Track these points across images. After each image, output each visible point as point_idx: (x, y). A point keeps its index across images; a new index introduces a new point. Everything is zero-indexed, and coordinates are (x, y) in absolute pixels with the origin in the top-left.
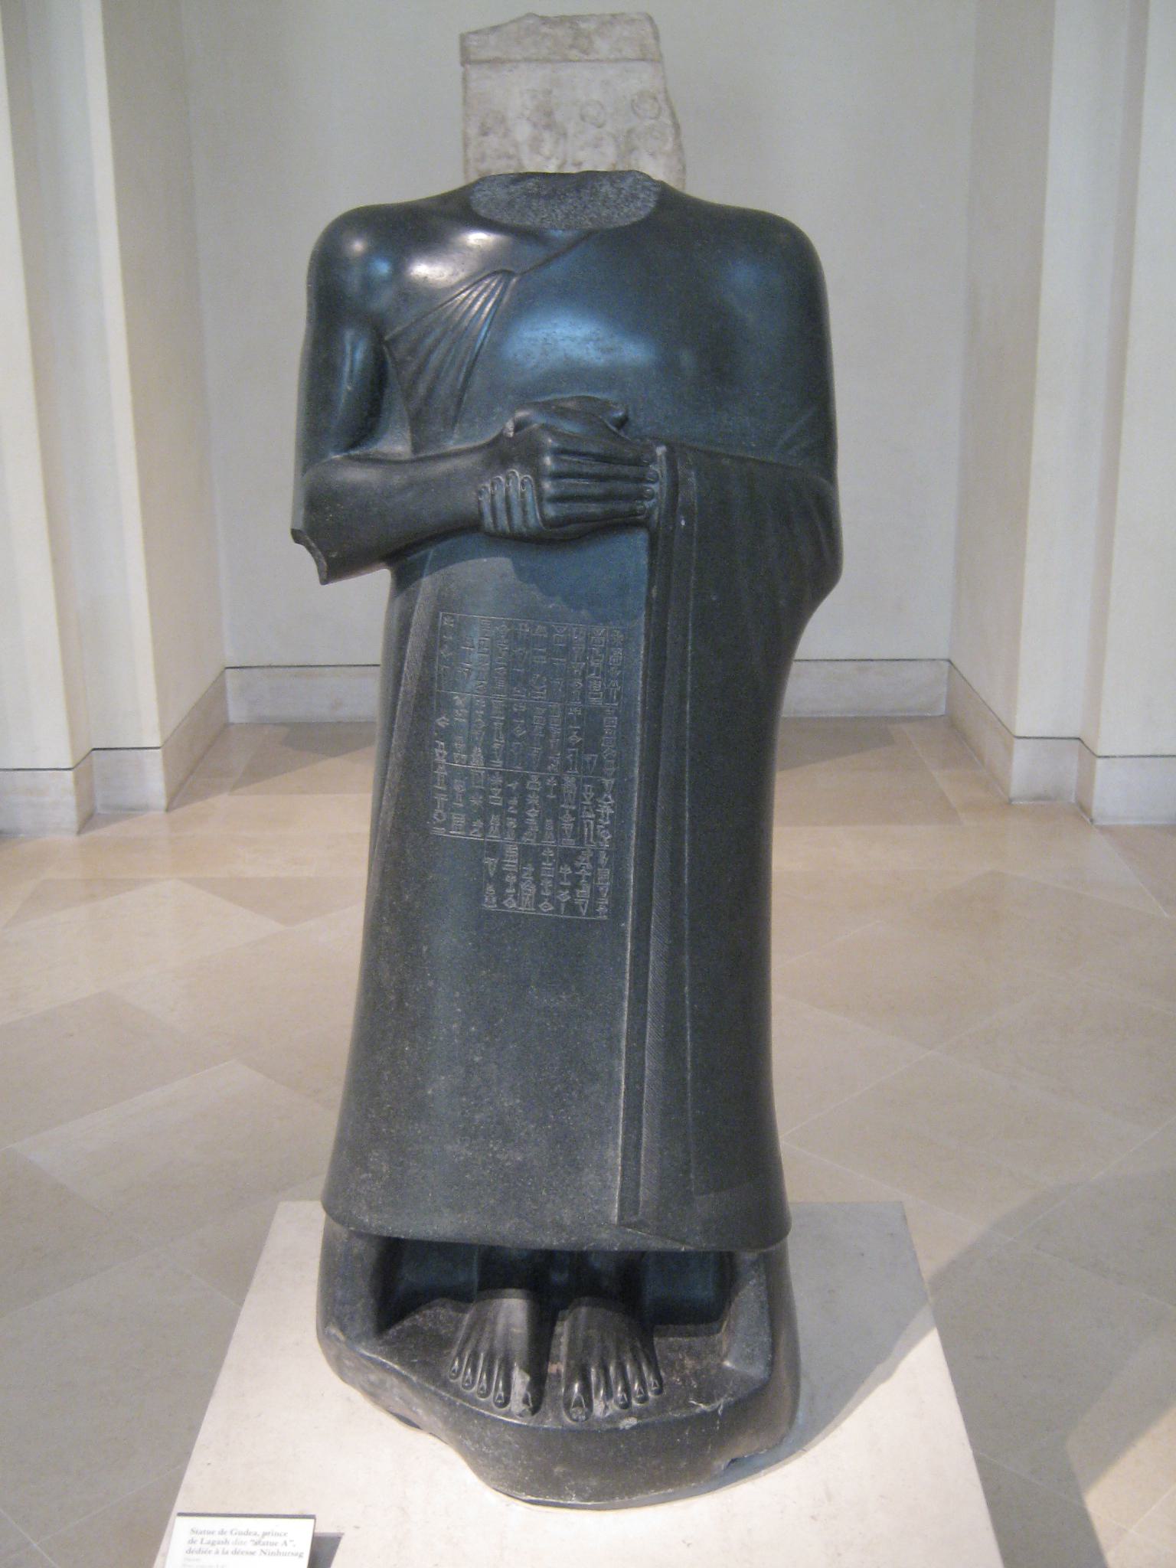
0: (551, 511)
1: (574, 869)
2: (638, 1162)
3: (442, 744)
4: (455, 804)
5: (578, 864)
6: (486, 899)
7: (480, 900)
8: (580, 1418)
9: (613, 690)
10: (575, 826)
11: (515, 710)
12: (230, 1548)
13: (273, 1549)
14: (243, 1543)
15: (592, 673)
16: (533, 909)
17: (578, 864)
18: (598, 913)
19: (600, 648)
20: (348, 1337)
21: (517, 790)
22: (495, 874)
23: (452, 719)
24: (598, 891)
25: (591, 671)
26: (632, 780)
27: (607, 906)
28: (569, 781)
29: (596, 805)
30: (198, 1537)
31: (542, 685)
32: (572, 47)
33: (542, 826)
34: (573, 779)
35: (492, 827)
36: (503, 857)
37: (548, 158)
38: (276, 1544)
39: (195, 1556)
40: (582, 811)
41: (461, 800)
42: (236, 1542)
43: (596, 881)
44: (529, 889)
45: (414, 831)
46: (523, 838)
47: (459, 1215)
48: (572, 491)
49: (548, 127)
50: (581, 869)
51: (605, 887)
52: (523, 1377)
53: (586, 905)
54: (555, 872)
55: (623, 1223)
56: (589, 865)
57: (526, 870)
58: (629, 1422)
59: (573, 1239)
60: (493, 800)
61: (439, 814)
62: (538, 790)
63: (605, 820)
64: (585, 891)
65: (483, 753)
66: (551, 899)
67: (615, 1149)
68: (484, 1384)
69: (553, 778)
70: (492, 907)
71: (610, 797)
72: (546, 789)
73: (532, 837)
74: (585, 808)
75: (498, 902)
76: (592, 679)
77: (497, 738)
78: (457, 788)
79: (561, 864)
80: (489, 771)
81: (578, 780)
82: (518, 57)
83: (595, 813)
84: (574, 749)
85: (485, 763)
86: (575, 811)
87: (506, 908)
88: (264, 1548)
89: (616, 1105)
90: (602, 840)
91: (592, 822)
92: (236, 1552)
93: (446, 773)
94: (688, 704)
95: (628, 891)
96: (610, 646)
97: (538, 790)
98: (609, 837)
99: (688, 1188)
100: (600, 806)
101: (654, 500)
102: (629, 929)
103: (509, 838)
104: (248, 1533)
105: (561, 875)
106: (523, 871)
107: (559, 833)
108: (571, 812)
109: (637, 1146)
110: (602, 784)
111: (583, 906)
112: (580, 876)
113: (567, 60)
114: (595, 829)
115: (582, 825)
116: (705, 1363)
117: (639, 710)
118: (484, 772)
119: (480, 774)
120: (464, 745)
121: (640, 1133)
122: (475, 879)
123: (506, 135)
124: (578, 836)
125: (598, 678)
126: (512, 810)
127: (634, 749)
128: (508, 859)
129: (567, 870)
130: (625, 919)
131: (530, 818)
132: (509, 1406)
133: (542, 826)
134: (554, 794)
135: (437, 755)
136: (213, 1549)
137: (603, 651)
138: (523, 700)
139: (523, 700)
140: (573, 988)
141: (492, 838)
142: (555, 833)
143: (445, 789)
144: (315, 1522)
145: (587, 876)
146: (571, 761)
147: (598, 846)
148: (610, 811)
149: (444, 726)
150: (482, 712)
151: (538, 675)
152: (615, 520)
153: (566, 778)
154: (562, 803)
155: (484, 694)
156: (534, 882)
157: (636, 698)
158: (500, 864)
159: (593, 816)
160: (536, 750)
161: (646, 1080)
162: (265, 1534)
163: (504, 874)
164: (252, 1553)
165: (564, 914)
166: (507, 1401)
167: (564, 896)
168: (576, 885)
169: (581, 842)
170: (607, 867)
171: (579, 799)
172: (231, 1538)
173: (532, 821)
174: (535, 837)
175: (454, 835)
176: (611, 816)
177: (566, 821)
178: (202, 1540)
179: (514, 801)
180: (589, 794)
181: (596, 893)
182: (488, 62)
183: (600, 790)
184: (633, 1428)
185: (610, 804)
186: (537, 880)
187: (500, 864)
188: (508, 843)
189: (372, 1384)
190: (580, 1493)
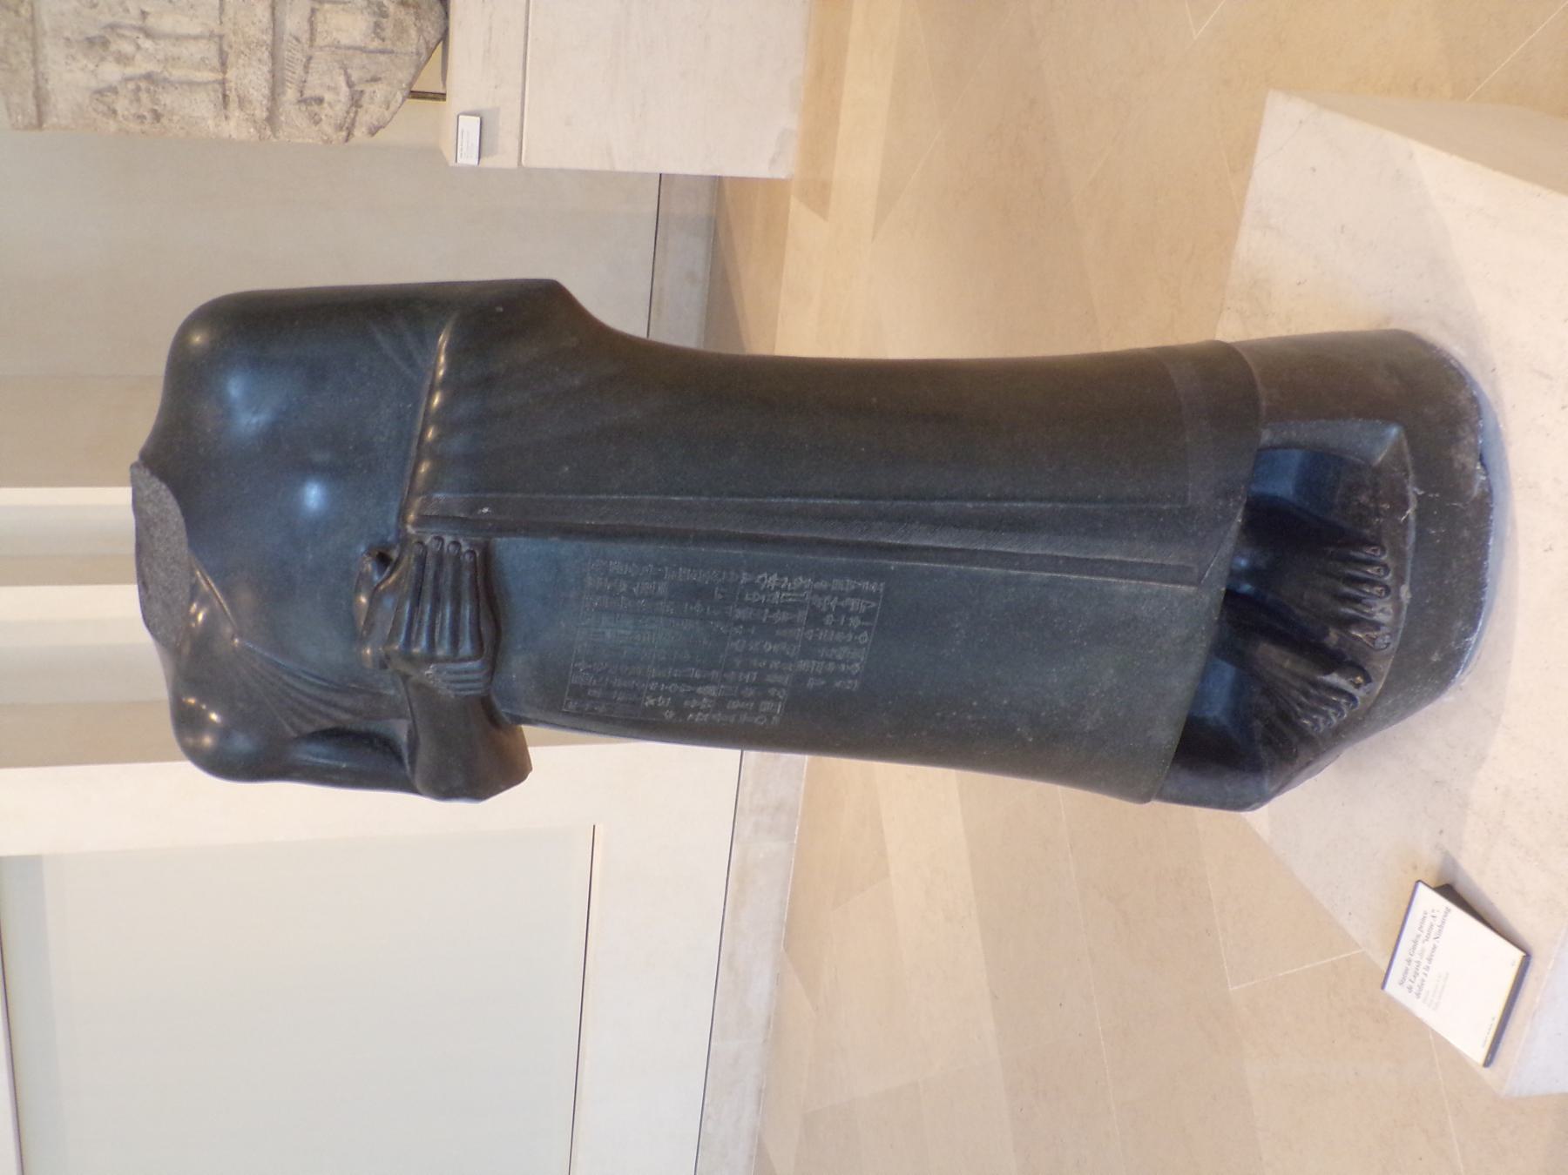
0: (466, 647)
2: (1140, 565)
5: (824, 609)
8: (1386, 641)
12: (1424, 963)
13: (1436, 929)
14: (1423, 950)
25: (631, 591)
27: (871, 582)
28: (740, 614)
29: (767, 590)
30: (1408, 983)
32: (17, 12)
33: (783, 639)
37: (138, 47)
38: (1432, 926)
39: (1423, 993)
42: (1421, 955)
47: (1157, 723)
49: (105, 43)
50: (829, 606)
51: (851, 584)
53: (868, 602)
55: (1198, 582)
56: (827, 598)
58: (1405, 593)
59: (1203, 628)
63: (783, 582)
64: (853, 603)
66: (857, 632)
67: (1121, 584)
69: (735, 629)
75: (853, 678)
79: (822, 625)
82: (32, 71)
83: (774, 591)
86: (770, 610)
88: (1433, 936)
89: (1075, 581)
90: (803, 585)
92: (1430, 960)
94: (673, 498)
99: (1176, 512)
100: (768, 586)
101: (461, 541)
104: (1415, 942)
107: (791, 624)
109: (1122, 564)
110: (747, 584)
111: (868, 605)
113: (33, 20)
114: (792, 591)
115: (787, 604)
116: (1367, 483)
121: (1109, 561)
123: (113, 90)
124: (793, 607)
129: (829, 619)
131: (772, 650)
132: (1358, 698)
133: (783, 639)
136: (1421, 975)
137: (611, 579)
144: (1423, 882)
145: (839, 600)
148: (775, 577)
152: (479, 583)
153: (737, 617)
158: (816, 676)
159: (777, 594)
161: (1056, 553)
162: (1420, 928)
164: (1435, 948)
167: (855, 622)
168: (846, 611)
170: (831, 582)
171: (759, 606)
172: (1416, 958)
173: (776, 648)
176: (780, 576)
178: (1410, 980)
180: (755, 597)
181: (856, 593)
182: (38, 106)
183: (752, 586)
184: (1412, 589)
186: (831, 645)
187: (816, 676)
190: (1466, 635)
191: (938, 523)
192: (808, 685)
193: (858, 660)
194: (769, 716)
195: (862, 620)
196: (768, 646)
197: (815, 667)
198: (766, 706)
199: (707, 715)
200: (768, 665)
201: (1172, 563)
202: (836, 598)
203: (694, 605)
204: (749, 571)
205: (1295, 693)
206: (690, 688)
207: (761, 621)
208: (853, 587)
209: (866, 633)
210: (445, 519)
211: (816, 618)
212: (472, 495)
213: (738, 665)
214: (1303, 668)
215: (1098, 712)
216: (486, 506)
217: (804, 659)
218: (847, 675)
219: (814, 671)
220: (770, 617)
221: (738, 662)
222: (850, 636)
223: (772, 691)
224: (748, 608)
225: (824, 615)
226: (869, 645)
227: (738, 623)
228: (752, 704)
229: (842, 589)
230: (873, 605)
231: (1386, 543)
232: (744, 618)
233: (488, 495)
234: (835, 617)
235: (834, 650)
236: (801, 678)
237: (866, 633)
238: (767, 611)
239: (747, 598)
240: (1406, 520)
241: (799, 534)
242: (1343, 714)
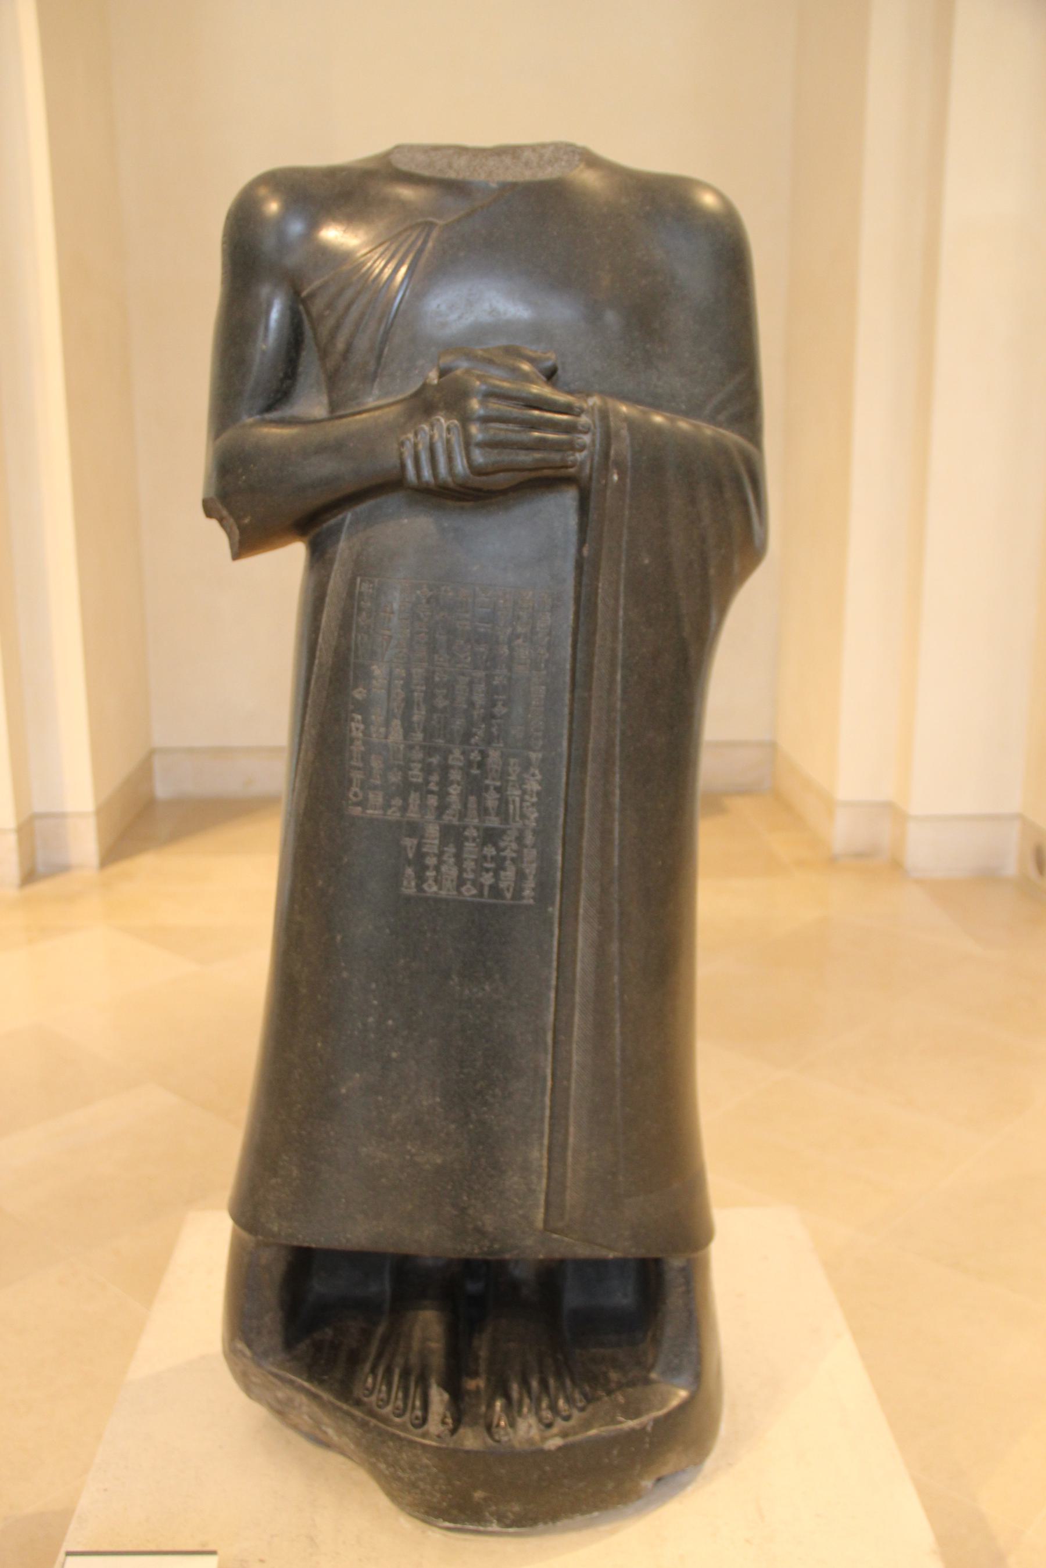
1: (499, 850)
20: (255, 1353)
25: (518, 637)
29: (521, 781)
33: (465, 805)
34: (498, 753)
43: (522, 862)
44: (450, 870)
48: (502, 436)
51: (531, 869)
52: (441, 1395)
56: (514, 846)
58: (554, 1443)
63: (532, 796)
64: (509, 874)
66: (474, 882)
67: (541, 1150)
68: (400, 1403)
69: (476, 752)
72: (470, 764)
73: (454, 816)
79: (484, 844)
83: (521, 788)
89: (542, 1101)
90: (528, 819)
101: (585, 453)
105: (485, 857)
107: (483, 811)
115: (507, 803)
124: (503, 811)
129: (490, 851)
133: (465, 805)
140: (497, 976)
142: (479, 811)
147: (524, 825)
148: (536, 787)
158: (419, 846)
159: (518, 792)
166: (424, 1420)
168: (500, 867)
170: (533, 847)
171: (504, 775)
176: (538, 794)
179: (435, 778)
180: (514, 768)
181: (521, 876)
183: (527, 765)
184: (560, 1449)
186: (459, 858)
187: (419, 846)
189: (279, 1401)
191: (600, 950)
192: (407, 839)
193: (440, 889)
194: (363, 804)
195: (491, 887)
196: (455, 789)
197: (431, 844)
198: (377, 798)
199: (361, 735)
200: (432, 792)
201: (568, 1197)
202: (514, 855)
203: (503, 705)
204: (543, 760)
205: (399, 1360)
207: (487, 778)
208: (527, 871)
209: (474, 892)
210: (608, 437)
211: (490, 836)
212: (629, 464)
213: (431, 760)
214: (437, 1361)
215: (385, 1156)
216: (620, 479)
217: (440, 831)
218: (421, 879)
219: (426, 844)
220: (492, 788)
221: (435, 760)
222: (471, 876)
223: (397, 802)
224: (501, 763)
225: (495, 845)
226: (461, 898)
227: (484, 754)
228: (378, 782)
229: (525, 859)
230: (509, 895)
231: (590, 1409)
232: (490, 760)
233: (628, 481)
234: (492, 858)
235: (452, 860)
236: (415, 829)
237: (474, 892)
238: (498, 784)
239: (512, 761)
240: (620, 1422)
241: (587, 807)
242: (399, 1416)
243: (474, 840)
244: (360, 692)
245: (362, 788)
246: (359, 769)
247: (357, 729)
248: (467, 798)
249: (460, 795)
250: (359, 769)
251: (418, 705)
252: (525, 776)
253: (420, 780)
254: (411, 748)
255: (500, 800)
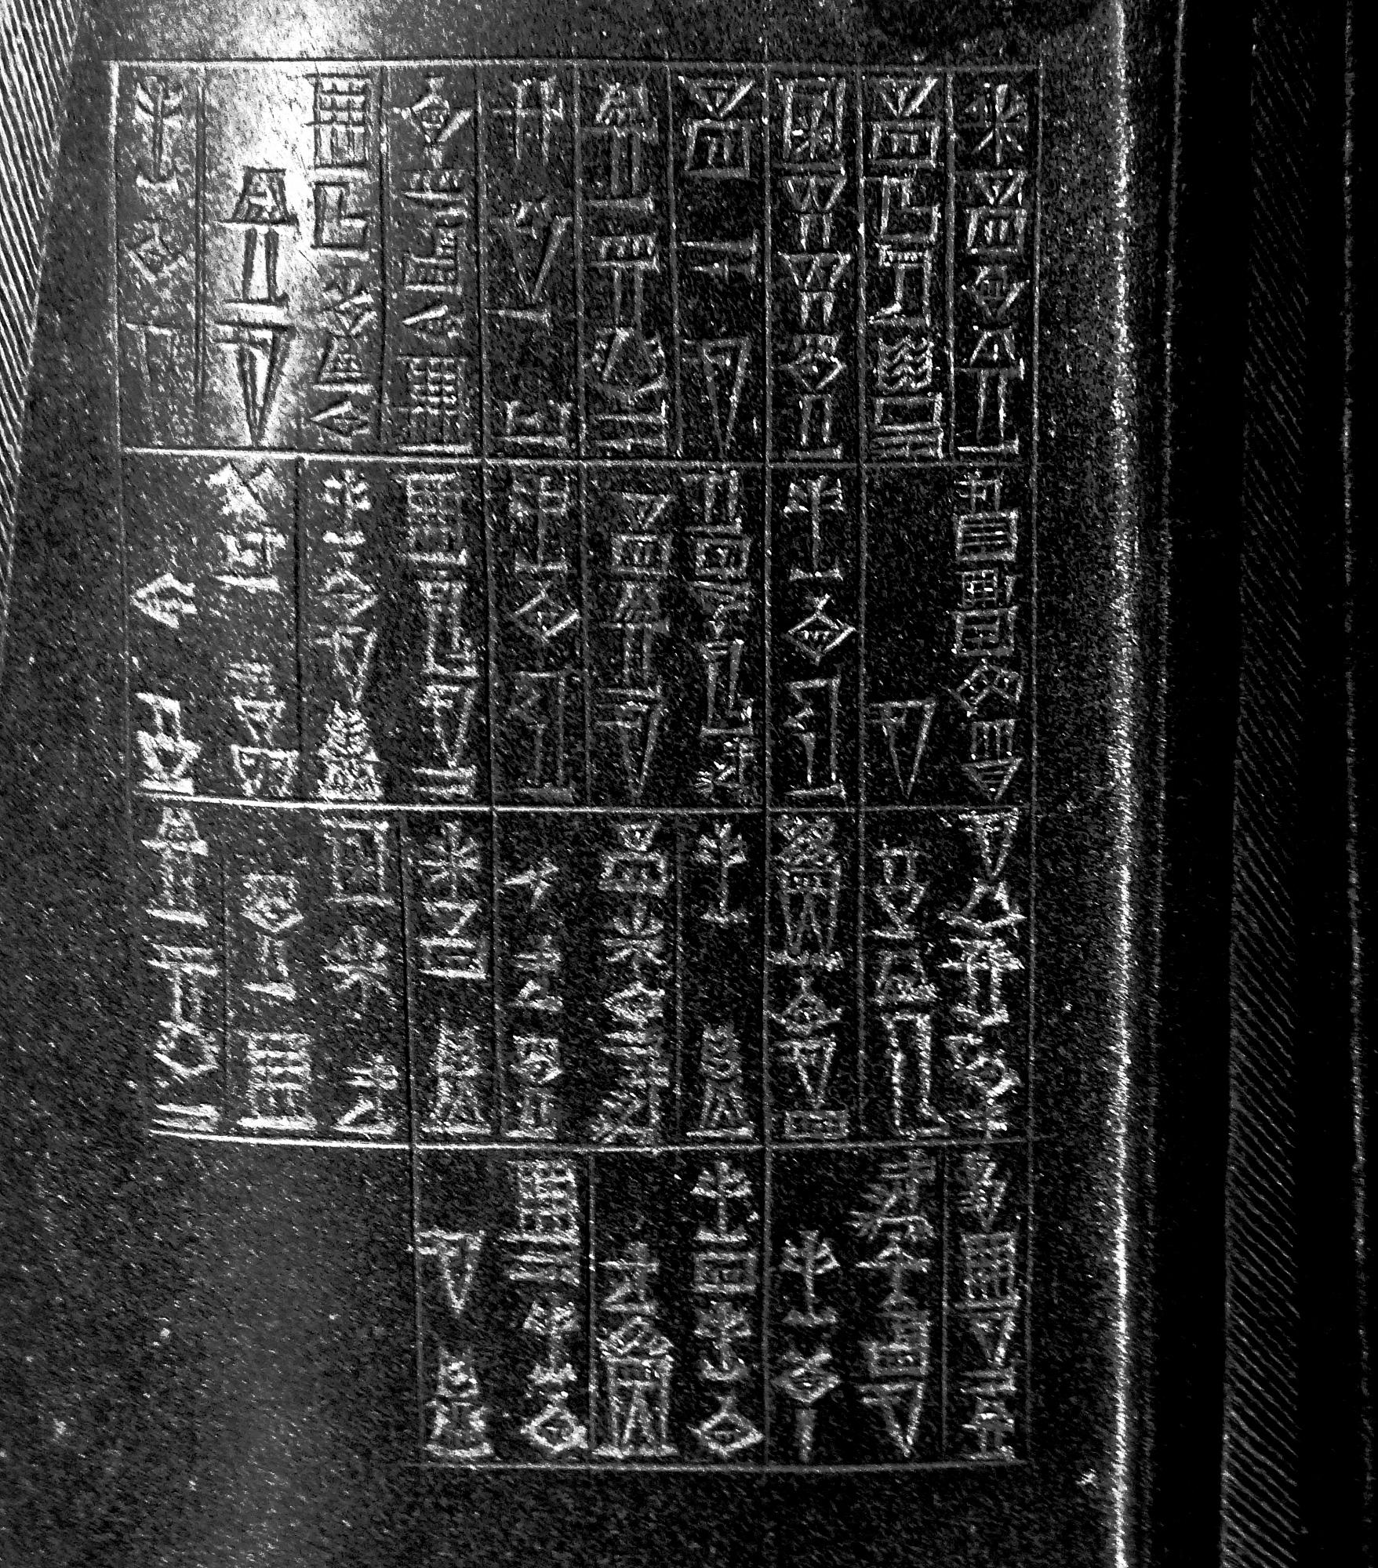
1: (851, 1247)
3: (173, 706)
4: (254, 987)
6: (441, 1421)
7: (416, 1426)
9: (993, 382)
10: (846, 1050)
11: (520, 511)
15: (889, 301)
16: (668, 1450)
17: (861, 1223)
18: (972, 1440)
19: (923, 171)
21: (551, 900)
22: (475, 1301)
23: (208, 586)
24: (970, 1339)
26: (1102, 810)
27: (1012, 1403)
31: (647, 380)
33: (691, 1076)
34: (823, 830)
35: (444, 1087)
36: (509, 1220)
40: (872, 971)
41: (283, 969)
43: (958, 1293)
45: (69, 1126)
46: (602, 1127)
50: (883, 1242)
54: (760, 1270)
56: (918, 1226)
57: (618, 1275)
60: (440, 957)
61: (184, 1038)
62: (658, 890)
65: (377, 739)
66: (750, 1398)
70: (474, 1453)
71: (1001, 896)
73: (641, 1119)
74: (889, 958)
75: (497, 1431)
76: (891, 335)
77: (440, 659)
78: (258, 912)
79: (786, 1229)
80: (414, 820)
81: (845, 826)
83: (934, 975)
84: (818, 683)
85: (388, 784)
86: (843, 976)
87: (539, 1453)
90: (975, 1099)
91: (922, 1022)
93: (200, 847)
95: (1105, 1325)
96: (968, 161)
97: (658, 890)
98: (1005, 1084)
102: (1119, 1492)
103: (525, 1131)
106: (605, 1280)
108: (823, 984)
110: (963, 845)
112: (883, 1276)
115: (878, 1035)
117: (1122, 466)
118: (384, 826)
119: (367, 838)
120: (280, 706)
122: (379, 1331)
125: (915, 323)
126: (534, 996)
127: (1103, 658)
128: (530, 1226)
130: (1099, 1454)
134: (732, 906)
135: (153, 762)
138: (558, 463)
139: (558, 463)
141: (446, 1138)
142: (751, 1088)
143: (200, 920)
146: (809, 738)
147: (957, 1128)
148: (1002, 962)
149: (173, 622)
150: (357, 539)
151: (623, 335)
153: (791, 827)
154: (778, 944)
155: (360, 448)
156: (661, 1326)
157: (1107, 413)
160: (634, 699)
163: (515, 1299)
165: (816, 1460)
169: (876, 1120)
173: (634, 1042)
174: (655, 1117)
175: (264, 1133)
176: (1012, 985)
177: (806, 1029)
185: (999, 932)
187: (494, 1261)
188: (530, 1156)
193: (600, 1437)
200: (536, 1023)
206: (458, 673)
239: (889, 854)
243: (737, 1212)
244: (167, 594)
245: (208, 1023)
246: (191, 936)
247: (169, 760)
248: (694, 1035)
249: (663, 1025)
250: (191, 936)
251: (444, 639)
252: (156, 601)
253: (477, 974)
254: (425, 829)
255: (843, 1032)
